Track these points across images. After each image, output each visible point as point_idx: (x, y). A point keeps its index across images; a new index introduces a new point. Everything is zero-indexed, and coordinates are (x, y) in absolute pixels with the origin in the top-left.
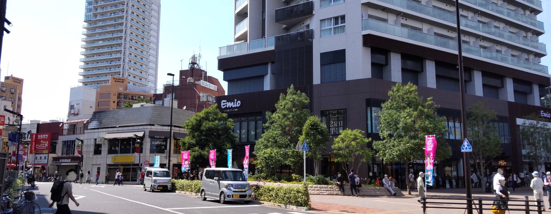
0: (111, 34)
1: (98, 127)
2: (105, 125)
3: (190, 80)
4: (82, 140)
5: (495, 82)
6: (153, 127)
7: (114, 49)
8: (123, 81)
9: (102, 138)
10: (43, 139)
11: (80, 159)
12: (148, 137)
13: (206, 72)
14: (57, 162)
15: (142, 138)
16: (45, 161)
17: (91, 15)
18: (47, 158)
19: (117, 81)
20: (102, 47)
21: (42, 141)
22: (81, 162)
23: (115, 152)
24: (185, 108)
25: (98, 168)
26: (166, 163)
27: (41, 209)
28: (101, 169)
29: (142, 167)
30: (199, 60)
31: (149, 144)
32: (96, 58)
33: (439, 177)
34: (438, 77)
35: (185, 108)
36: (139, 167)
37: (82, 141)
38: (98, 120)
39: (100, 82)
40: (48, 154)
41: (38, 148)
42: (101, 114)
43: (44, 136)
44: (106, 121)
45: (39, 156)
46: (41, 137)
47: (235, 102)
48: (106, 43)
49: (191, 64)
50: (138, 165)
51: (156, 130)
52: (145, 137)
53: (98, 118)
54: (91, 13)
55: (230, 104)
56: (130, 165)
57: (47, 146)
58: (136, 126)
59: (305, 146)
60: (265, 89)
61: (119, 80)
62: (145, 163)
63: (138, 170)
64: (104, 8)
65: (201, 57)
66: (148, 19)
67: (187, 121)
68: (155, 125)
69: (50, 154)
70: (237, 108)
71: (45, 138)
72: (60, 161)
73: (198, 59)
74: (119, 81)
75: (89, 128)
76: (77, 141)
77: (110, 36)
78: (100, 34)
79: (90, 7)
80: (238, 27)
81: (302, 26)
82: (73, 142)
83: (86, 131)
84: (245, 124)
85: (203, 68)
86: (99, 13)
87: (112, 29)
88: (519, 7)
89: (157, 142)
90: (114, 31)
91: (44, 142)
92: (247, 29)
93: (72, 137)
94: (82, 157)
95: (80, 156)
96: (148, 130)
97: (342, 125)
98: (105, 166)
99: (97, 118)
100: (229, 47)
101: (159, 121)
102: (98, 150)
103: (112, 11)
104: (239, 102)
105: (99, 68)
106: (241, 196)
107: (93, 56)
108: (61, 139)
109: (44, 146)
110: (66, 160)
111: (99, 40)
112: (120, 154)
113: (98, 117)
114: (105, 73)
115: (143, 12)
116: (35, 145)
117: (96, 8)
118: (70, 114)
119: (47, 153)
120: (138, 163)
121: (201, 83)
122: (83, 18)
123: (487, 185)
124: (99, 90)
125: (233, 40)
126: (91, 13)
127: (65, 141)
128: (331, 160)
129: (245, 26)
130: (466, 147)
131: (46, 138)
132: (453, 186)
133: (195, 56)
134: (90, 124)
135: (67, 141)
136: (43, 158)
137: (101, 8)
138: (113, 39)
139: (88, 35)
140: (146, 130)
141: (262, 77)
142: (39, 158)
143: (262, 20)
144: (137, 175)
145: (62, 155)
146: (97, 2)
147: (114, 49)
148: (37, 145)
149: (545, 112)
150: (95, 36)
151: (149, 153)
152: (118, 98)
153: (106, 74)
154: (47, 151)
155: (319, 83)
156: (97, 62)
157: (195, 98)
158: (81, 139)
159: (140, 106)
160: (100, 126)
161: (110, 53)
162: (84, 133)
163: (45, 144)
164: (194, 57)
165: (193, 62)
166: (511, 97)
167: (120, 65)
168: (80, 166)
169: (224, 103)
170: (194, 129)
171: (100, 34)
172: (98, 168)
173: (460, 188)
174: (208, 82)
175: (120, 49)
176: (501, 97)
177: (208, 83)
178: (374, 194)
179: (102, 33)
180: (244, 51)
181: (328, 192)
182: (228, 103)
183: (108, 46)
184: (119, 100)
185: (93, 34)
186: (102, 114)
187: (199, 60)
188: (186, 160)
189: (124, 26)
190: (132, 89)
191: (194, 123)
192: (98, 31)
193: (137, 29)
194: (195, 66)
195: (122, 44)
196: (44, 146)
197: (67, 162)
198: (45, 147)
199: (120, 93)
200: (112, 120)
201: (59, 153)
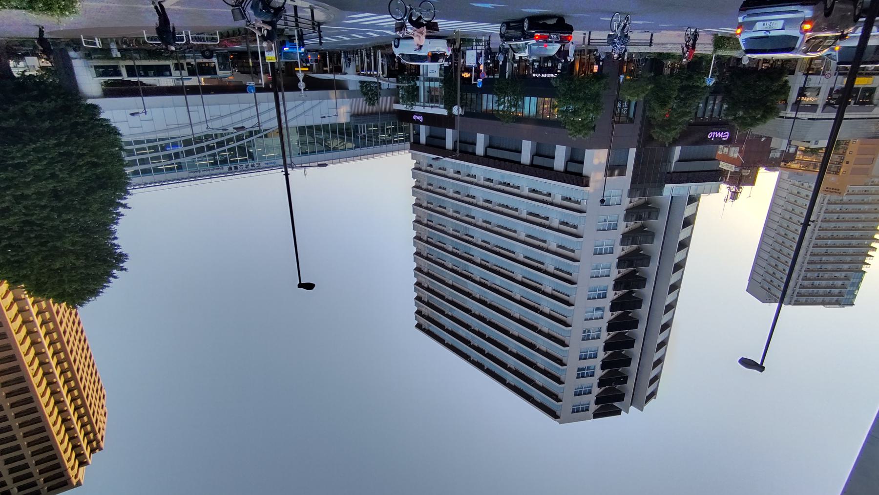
6: (811, 117)
27: (189, 107)
39: (861, 193)
42: (874, 136)
50: (840, 74)
52: (822, 106)
55: (720, 135)
61: (832, 190)
64: (832, 285)
74: (833, 189)
80: (694, 212)
89: (809, 100)
103: (820, 280)
104: (709, 137)
120: (839, 77)
121: (734, 168)
122: (866, 277)
129: (688, 211)
141: (679, 161)
146: (843, 285)
149: (418, 121)
155: (630, 149)
159: (820, 141)
169: (725, 137)
170: (771, 108)
176: (457, 132)
194: (734, 190)
199: (836, 174)
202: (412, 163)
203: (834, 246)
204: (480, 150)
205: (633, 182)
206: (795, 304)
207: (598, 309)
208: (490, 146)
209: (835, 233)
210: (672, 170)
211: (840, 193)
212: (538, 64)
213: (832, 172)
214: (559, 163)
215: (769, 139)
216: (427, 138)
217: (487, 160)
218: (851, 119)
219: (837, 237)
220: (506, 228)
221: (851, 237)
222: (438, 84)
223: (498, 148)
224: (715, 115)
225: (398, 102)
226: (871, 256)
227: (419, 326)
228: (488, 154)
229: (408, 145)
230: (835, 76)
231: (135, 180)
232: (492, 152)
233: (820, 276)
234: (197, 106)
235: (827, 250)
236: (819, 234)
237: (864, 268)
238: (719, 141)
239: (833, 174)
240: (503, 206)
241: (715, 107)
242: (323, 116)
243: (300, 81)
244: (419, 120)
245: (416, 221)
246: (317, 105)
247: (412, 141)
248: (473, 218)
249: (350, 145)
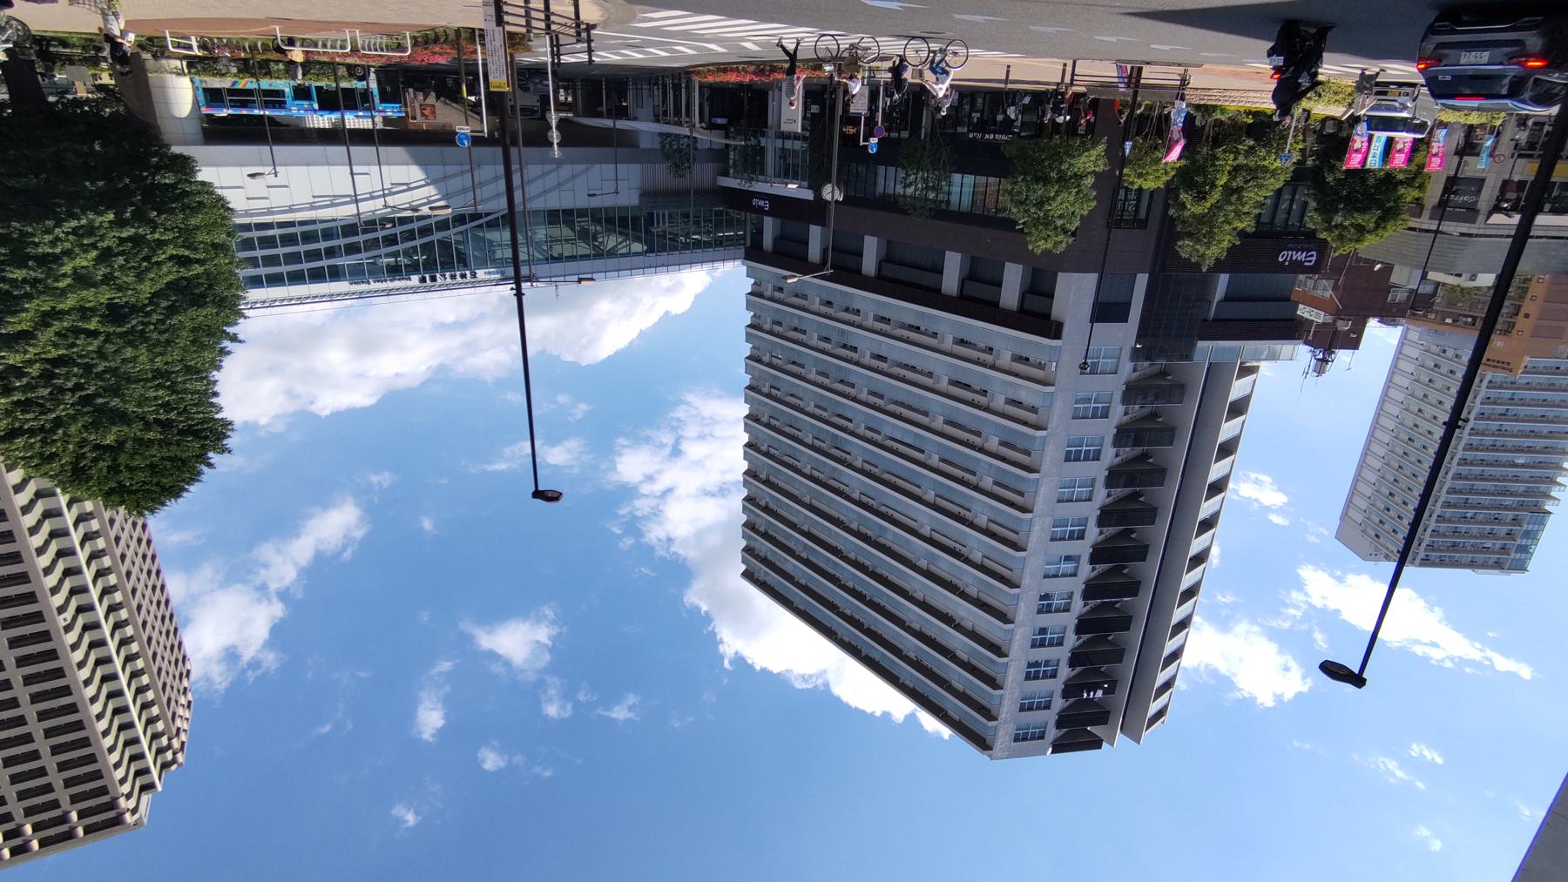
3: (1344, 326)
6: (1465, 230)
7: (1488, 440)
15: (1496, 209)
17: (1528, 524)
20: (1519, 450)
29: (1512, 151)
32: (1545, 428)
34: (939, 271)
35: (1378, 267)
48: (1504, 456)
50: (1521, 156)
55: (1300, 256)
58: (1501, 236)
66: (1381, 494)
67: (1386, 234)
78: (1516, 479)
79: (1524, 542)
80: (1248, 391)
86: (1505, 524)
87: (1479, 484)
90: (1476, 479)
100: (1273, 357)
104: (1280, 260)
106: (1385, 93)
111: (1522, 466)
114: (1529, 389)
115: (1388, 510)
122: (1551, 522)
125: (1261, 370)
129: (1238, 388)
138: (1482, 462)
139: (1552, 481)
140: (1482, 225)
141: (1228, 298)
153: (1528, 386)
156: (1543, 418)
161: (1500, 432)
164: (1320, 371)
166: (815, 233)
169: (1310, 261)
171: (1516, 479)
179: (1510, 481)
180: (1250, 346)
181: (1210, 93)
183: (1504, 449)
184: (1510, 320)
185: (1535, 482)
188: (1436, 155)
189: (1442, 499)
191: (655, 533)
192: (1521, 487)
193: (1414, 475)
194: (1321, 356)
200: (1553, 253)
202: (748, 284)
204: (869, 265)
206: (1421, 565)
207: (1068, 558)
208: (885, 260)
211: (1511, 371)
212: (978, 115)
214: (1010, 295)
215: (1388, 269)
216: (775, 240)
217: (881, 284)
220: (909, 407)
223: (901, 263)
224: (1294, 221)
225: (726, 174)
227: (748, 575)
228: (883, 273)
229: (742, 251)
230: (1512, 160)
231: (254, 294)
232: (891, 271)
234: (369, 164)
238: (1297, 267)
240: (906, 366)
241: (1294, 207)
242: (591, 192)
243: (551, 128)
244: (763, 208)
245: (750, 388)
246: (580, 174)
247: (749, 244)
248: (852, 386)
249: (637, 247)
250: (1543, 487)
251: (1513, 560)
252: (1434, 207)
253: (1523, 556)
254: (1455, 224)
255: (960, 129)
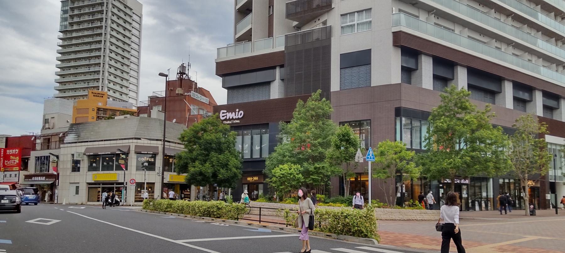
0: (88, 68)
1: (76, 141)
2: (84, 139)
3: (179, 91)
4: (58, 155)
5: (525, 96)
6: (139, 141)
8: (102, 95)
9: (80, 153)
10: (13, 155)
11: (57, 177)
12: (133, 152)
13: (196, 83)
14: (29, 180)
16: (16, 180)
18: (17, 176)
19: (96, 96)
21: (11, 157)
22: (57, 181)
23: (96, 169)
24: (174, 121)
25: (76, 187)
26: (154, 182)
28: (79, 189)
30: (188, 70)
31: (135, 160)
33: (492, 197)
35: (174, 121)
36: (124, 186)
37: (57, 157)
38: (76, 133)
40: (18, 172)
41: (7, 164)
42: (78, 126)
43: (14, 151)
44: (84, 134)
45: (8, 173)
46: (9, 152)
47: (237, 113)
49: (180, 75)
50: (122, 184)
51: (142, 145)
52: (131, 152)
53: (76, 131)
54: (67, 23)
55: (230, 115)
56: (113, 184)
57: (18, 162)
59: (371, 155)
60: (272, 97)
61: (98, 95)
62: (131, 182)
63: (123, 190)
65: (190, 66)
68: (141, 139)
69: (20, 171)
70: (238, 119)
71: (15, 153)
72: (33, 179)
73: (187, 69)
74: (98, 96)
75: (65, 142)
76: (52, 157)
77: (88, 47)
80: (239, 25)
81: (318, 22)
82: (48, 158)
83: (62, 146)
84: (248, 138)
85: (192, 79)
88: (525, 24)
89: (144, 158)
91: (15, 158)
92: (252, 26)
93: (46, 153)
94: (58, 174)
95: (56, 173)
96: (134, 144)
97: (364, 139)
98: (85, 185)
99: (74, 130)
101: (145, 135)
102: (76, 167)
105: (77, 74)
107: (70, 69)
108: (33, 155)
109: (14, 162)
110: (40, 177)
112: (102, 171)
113: (75, 129)
116: (3, 161)
117: (73, 17)
118: (44, 128)
119: (18, 170)
120: (123, 182)
123: (531, 207)
124: (76, 105)
126: (67, 23)
127: (38, 157)
128: (362, 179)
130: (371, 157)
131: (16, 153)
132: (483, 209)
133: (184, 65)
134: (66, 137)
135: (41, 157)
136: (13, 175)
137: (78, 17)
141: (268, 83)
142: (8, 176)
143: (269, 17)
144: (121, 195)
145: (35, 172)
146: (72, 18)
147: (93, 54)
148: (6, 161)
150: (71, 47)
151: (135, 171)
152: (97, 114)
154: (18, 168)
157: (185, 111)
158: (56, 154)
160: (78, 139)
161: (89, 58)
162: (59, 148)
163: (15, 160)
165: (182, 72)
167: (99, 79)
168: (56, 185)
169: (223, 113)
172: (76, 187)
173: (489, 210)
174: (199, 93)
175: (99, 62)
177: (199, 95)
178: (420, 219)
182: (228, 113)
186: (80, 127)
187: (188, 70)
190: (111, 104)
195: (101, 49)
196: (14, 162)
197: (41, 181)
198: (15, 163)
199: (99, 108)
201: (31, 169)
203: (84, 74)
205: (326, 49)
209: (87, 62)
210: (278, 70)
213: (102, 109)
218: (102, 141)
219: (85, 74)
221: (77, 60)
222: (550, 170)
224: (257, 138)
226: (59, 46)
233: (90, 24)
235: (88, 85)
236: (99, 60)
237: (61, 35)
239: (101, 108)
250: (66, 43)
251: (68, 6)
252: (158, 154)
253: (63, 24)
254: (145, 145)
255: (270, 193)
